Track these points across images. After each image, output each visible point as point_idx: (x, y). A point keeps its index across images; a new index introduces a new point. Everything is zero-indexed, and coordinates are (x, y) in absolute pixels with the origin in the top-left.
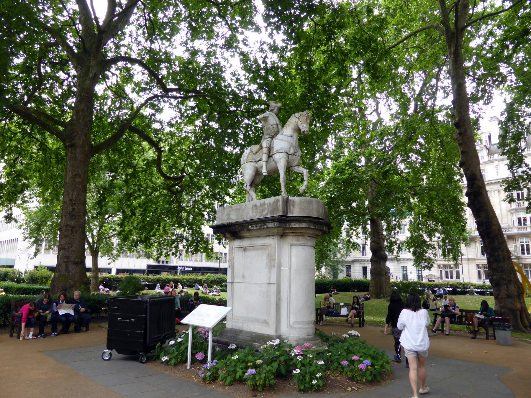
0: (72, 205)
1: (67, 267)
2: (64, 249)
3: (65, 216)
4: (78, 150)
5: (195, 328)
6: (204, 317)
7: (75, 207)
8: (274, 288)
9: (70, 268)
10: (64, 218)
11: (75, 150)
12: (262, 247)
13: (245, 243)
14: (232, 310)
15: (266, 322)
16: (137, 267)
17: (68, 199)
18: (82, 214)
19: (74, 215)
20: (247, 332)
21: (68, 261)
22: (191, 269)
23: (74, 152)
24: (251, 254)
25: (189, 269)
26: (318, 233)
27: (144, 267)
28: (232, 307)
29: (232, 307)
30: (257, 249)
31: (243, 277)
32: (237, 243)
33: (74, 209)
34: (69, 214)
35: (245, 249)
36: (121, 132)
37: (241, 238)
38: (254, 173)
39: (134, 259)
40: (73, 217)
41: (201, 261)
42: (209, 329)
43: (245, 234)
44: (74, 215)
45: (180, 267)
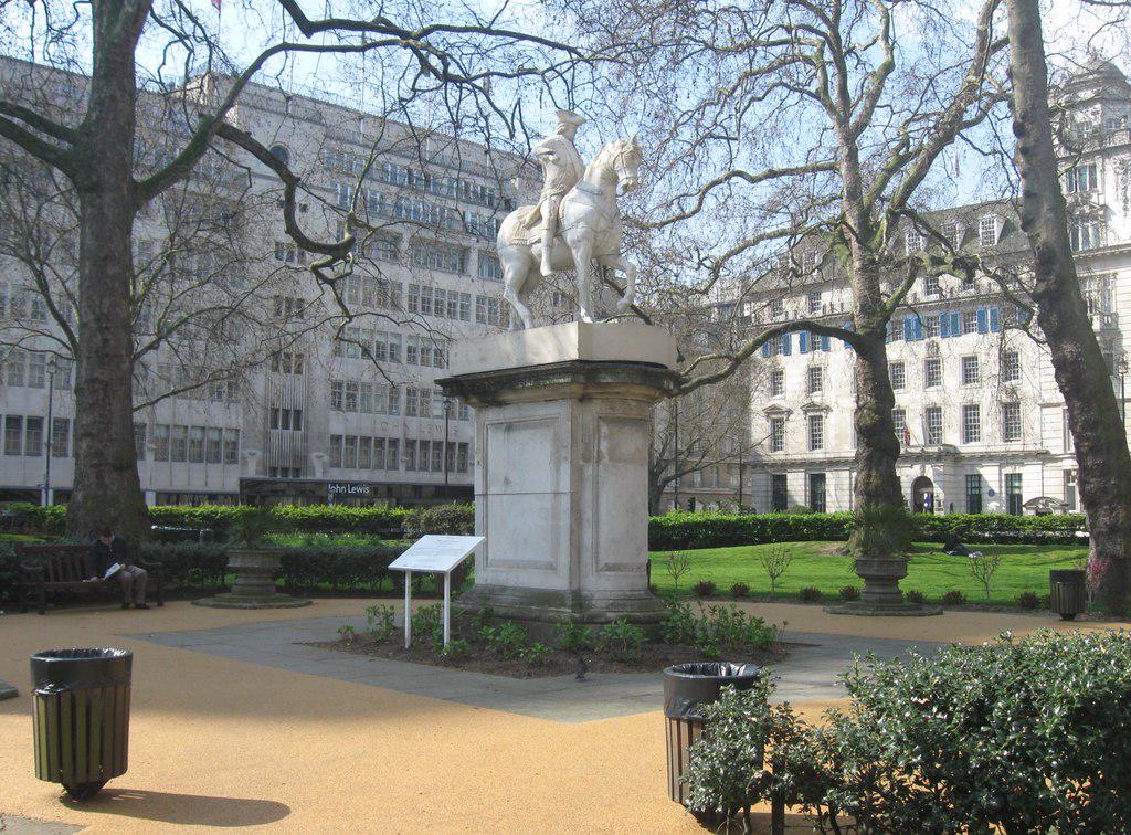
0: (101, 330)
1: (99, 477)
2: (90, 435)
3: (88, 358)
4: (108, 197)
5: (417, 574)
6: (432, 554)
7: (110, 337)
8: (565, 502)
9: (107, 481)
10: (85, 361)
11: (100, 197)
12: (543, 423)
13: (508, 414)
14: (485, 544)
15: (552, 567)
16: (215, 486)
17: (91, 317)
18: (123, 352)
19: (107, 355)
20: (515, 589)
21: (100, 465)
22: (367, 490)
23: (98, 201)
24: (520, 436)
25: (360, 490)
26: (652, 393)
27: (232, 486)
28: (487, 536)
29: (487, 536)
30: (998, 611)
31: (507, 481)
32: (493, 415)
33: (105, 341)
34: (97, 352)
35: (509, 427)
36: (200, 144)
37: (501, 404)
38: (527, 269)
39: (203, 465)
40: (106, 360)
41: (395, 468)
42: (440, 576)
43: (509, 396)
44: (107, 355)
45: (334, 484)
